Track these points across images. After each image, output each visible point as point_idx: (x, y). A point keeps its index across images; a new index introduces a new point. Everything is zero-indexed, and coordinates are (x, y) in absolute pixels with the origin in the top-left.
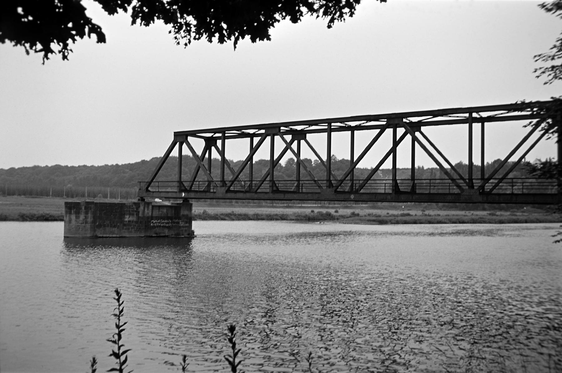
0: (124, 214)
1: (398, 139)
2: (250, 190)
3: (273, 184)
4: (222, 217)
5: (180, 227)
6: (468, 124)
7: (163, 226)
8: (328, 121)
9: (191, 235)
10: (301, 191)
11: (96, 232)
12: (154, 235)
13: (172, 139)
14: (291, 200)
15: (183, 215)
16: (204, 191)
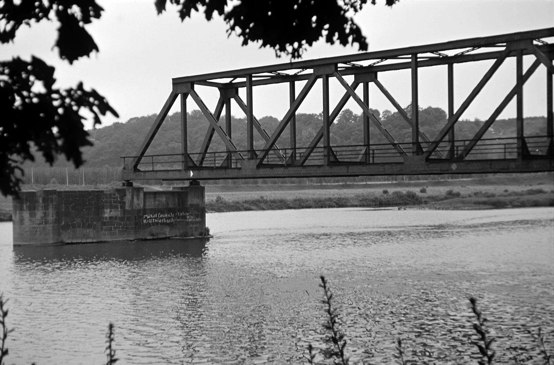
0: (103, 208)
1: (524, 72)
2: (292, 163)
3: (328, 153)
4: (246, 205)
5: (188, 223)
6: (410, 70)
7: (161, 224)
8: (412, 51)
9: (204, 236)
10: (371, 162)
11: (62, 236)
12: (148, 238)
13: (169, 89)
14: (358, 176)
15: (192, 205)
16: (221, 168)
